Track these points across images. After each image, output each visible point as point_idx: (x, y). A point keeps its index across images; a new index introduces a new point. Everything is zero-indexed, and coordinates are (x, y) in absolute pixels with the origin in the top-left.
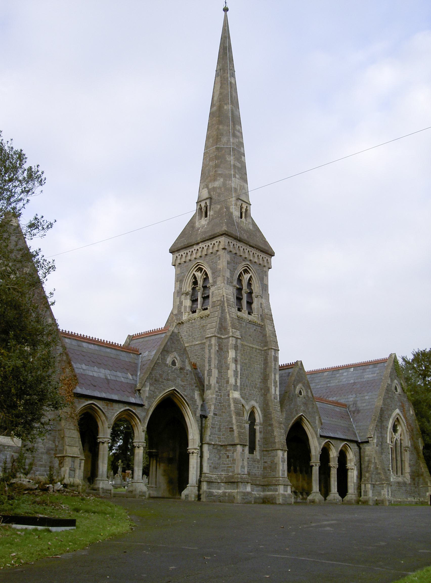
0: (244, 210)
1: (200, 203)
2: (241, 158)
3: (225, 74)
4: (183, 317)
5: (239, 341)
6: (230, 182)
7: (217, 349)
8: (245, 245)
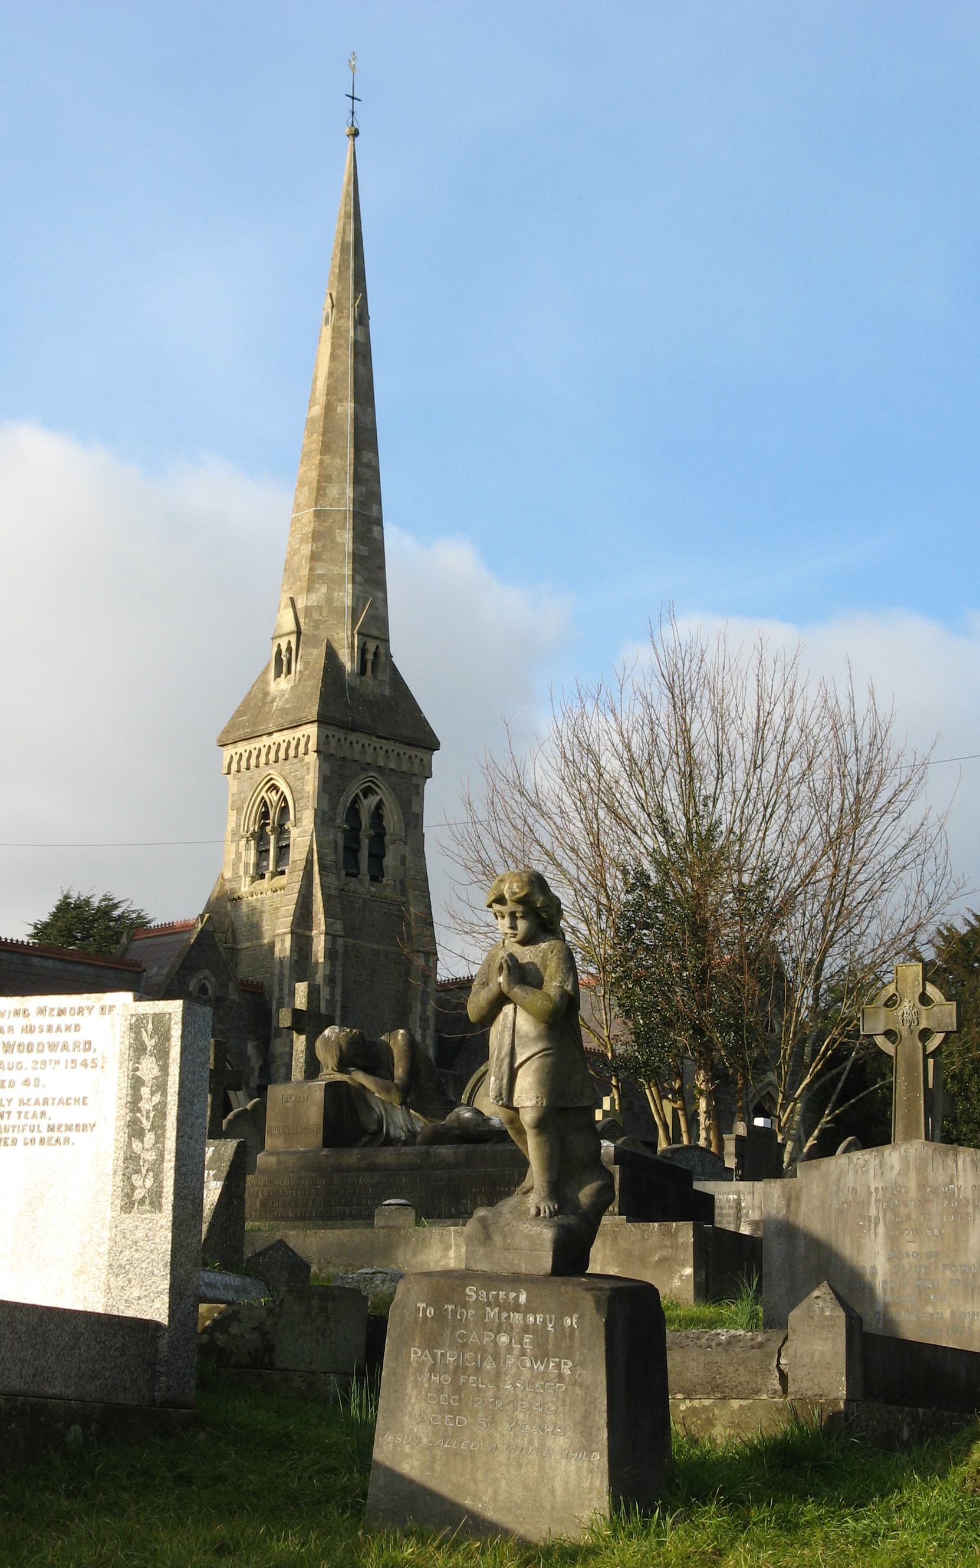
0: (370, 656)
1: (278, 641)
2: (370, 531)
3: (342, 321)
4: (243, 886)
5: (340, 941)
6: (341, 594)
7: (296, 958)
8: (367, 736)
